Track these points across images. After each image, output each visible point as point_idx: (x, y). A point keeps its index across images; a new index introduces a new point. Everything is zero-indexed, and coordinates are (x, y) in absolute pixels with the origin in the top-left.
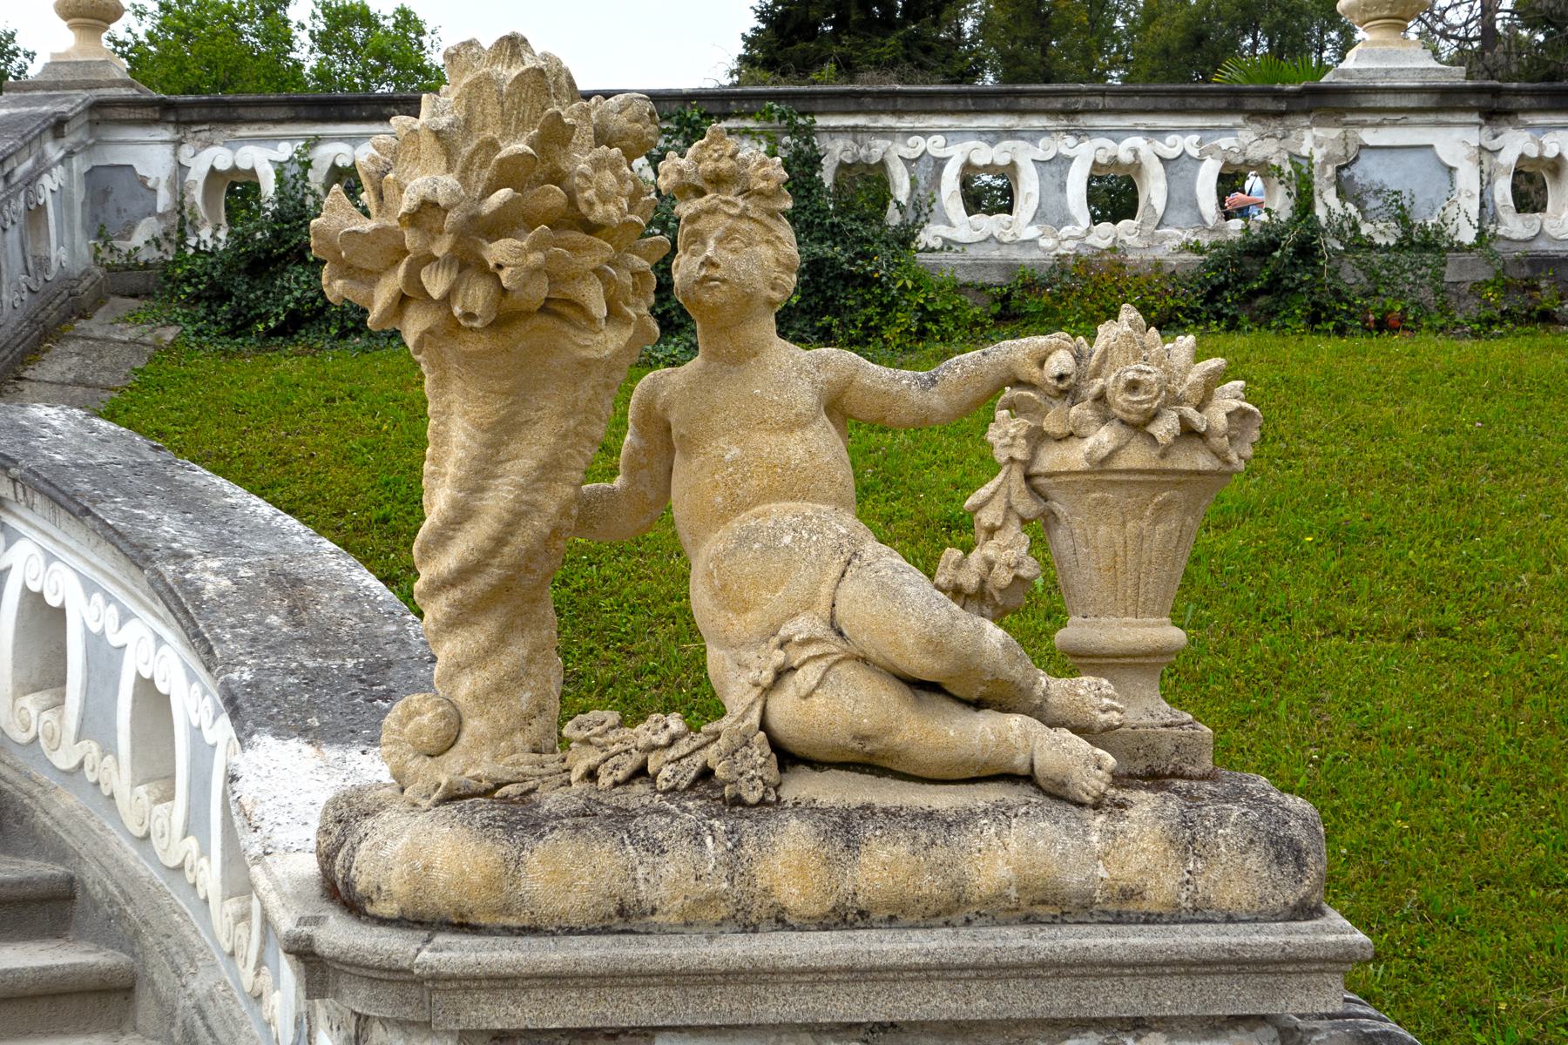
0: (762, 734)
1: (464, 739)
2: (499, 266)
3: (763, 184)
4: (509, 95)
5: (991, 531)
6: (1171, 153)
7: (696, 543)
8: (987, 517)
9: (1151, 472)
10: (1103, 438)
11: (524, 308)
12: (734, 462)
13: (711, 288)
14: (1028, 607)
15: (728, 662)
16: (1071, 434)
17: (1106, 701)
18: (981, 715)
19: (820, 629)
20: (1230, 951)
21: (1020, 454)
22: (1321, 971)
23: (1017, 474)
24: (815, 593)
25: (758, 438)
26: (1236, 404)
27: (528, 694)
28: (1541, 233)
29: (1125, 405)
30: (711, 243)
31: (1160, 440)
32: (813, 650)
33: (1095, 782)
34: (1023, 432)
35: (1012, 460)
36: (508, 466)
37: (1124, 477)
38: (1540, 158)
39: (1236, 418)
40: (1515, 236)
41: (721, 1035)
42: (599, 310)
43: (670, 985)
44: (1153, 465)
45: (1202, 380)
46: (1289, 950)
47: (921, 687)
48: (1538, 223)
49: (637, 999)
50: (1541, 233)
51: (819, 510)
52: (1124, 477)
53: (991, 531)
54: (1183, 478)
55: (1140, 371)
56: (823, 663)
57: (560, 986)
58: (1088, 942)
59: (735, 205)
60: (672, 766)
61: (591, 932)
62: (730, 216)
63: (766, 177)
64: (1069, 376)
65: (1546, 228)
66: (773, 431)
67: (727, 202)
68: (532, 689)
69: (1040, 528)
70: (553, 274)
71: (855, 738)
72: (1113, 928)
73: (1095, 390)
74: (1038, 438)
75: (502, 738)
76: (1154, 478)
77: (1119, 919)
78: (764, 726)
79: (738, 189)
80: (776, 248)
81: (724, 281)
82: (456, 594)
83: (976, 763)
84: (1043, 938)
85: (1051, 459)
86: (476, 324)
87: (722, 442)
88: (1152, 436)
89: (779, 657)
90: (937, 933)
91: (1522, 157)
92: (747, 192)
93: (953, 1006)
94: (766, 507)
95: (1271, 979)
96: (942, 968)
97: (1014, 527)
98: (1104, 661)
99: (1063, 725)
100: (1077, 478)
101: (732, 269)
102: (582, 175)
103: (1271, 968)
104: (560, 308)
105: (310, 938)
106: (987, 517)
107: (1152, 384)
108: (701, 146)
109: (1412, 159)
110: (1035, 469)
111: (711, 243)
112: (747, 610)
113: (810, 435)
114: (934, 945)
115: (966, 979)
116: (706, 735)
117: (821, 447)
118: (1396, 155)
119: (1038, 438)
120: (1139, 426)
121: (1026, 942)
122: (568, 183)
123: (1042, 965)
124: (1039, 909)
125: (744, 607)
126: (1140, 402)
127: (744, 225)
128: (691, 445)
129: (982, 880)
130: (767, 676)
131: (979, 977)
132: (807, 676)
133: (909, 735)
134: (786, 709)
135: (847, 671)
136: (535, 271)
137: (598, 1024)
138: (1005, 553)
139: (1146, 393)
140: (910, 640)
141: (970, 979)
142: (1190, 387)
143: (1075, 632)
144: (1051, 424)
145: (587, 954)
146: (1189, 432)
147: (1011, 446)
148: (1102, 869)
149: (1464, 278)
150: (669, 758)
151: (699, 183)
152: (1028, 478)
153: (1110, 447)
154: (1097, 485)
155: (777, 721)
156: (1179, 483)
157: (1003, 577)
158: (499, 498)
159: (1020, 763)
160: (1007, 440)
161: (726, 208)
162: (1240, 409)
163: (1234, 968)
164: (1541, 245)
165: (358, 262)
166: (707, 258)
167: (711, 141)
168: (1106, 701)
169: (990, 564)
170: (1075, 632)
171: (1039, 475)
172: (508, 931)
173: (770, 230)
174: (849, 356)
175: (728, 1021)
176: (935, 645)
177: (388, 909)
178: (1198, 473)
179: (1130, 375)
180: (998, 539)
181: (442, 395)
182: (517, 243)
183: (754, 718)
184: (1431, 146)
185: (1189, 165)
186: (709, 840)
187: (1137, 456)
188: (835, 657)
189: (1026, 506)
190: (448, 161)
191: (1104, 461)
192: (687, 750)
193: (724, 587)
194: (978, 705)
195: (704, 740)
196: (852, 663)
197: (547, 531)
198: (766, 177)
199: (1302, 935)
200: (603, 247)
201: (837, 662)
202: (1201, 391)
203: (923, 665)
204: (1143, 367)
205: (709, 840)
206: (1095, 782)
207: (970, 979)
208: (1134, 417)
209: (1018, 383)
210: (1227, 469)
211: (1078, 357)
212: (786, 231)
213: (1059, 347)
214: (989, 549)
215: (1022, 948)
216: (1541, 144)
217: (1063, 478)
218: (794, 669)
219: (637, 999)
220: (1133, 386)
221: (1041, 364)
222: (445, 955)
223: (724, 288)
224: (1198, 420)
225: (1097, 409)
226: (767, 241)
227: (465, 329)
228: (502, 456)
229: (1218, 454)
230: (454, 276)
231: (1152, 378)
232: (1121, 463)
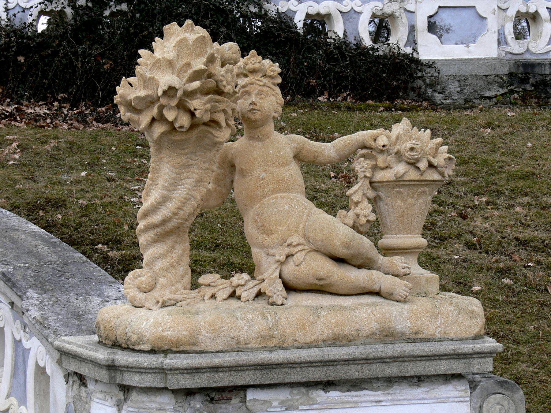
0: (280, 280)
1: (158, 286)
2: (195, 109)
3: (272, 74)
4: (193, 45)
5: (357, 203)
6: (345, 9)
7: (247, 209)
8: (355, 198)
9: (418, 181)
10: (400, 168)
11: (197, 123)
12: (264, 179)
13: (254, 113)
14: (374, 230)
15: (263, 254)
16: (387, 167)
17: (405, 265)
18: (361, 270)
19: (302, 240)
20: (454, 350)
21: (368, 175)
22: (485, 357)
23: (367, 182)
24: (298, 227)
25: (272, 170)
26: (447, 155)
27: (182, 268)
28: (528, 50)
29: (409, 156)
30: (253, 96)
31: (421, 169)
32: (300, 248)
33: (405, 293)
34: (370, 166)
35: (365, 177)
36: (184, 181)
37: (408, 183)
38: (527, 13)
39: (447, 160)
40: (515, 52)
41: (271, 388)
42: (223, 124)
43: (256, 369)
44: (418, 178)
45: (435, 146)
46: (475, 349)
47: (339, 260)
48: (526, 45)
49: (244, 375)
50: (528, 50)
51: (295, 196)
52: (408, 183)
53: (357, 203)
54: (429, 183)
55: (414, 144)
56: (304, 253)
57: (217, 371)
58: (405, 349)
59: (261, 81)
60: (246, 292)
61: (226, 351)
62: (260, 85)
63: (273, 71)
64: (387, 145)
65: (530, 48)
66: (277, 167)
67: (258, 80)
68: (183, 266)
69: (374, 201)
70: (212, 111)
71: (317, 279)
72: (413, 344)
73: (395, 150)
74: (375, 168)
75: (173, 285)
76: (418, 183)
77: (414, 341)
78: (280, 277)
79: (261, 75)
80: (276, 97)
81: (259, 110)
82: (159, 230)
83: (360, 288)
84: (389, 348)
85: (380, 176)
86: (183, 130)
87: (258, 171)
88: (418, 168)
89: (287, 251)
90: (351, 348)
91: (518, 12)
92: (264, 76)
93: (357, 374)
94: (276, 195)
95: (468, 360)
96: (355, 360)
97: (366, 202)
98: (399, 251)
99: (389, 274)
100: (390, 183)
101: (261, 106)
102: (223, 76)
103: (469, 356)
104: (214, 123)
105: (113, 360)
106: (355, 198)
107: (418, 149)
108: (248, 59)
109: (465, 14)
110: (373, 180)
111: (253, 96)
112: (272, 234)
113: (291, 168)
114: (352, 351)
115: (362, 364)
116: (258, 280)
117: (293, 172)
118: (457, 11)
119: (375, 168)
120: (413, 164)
121: (384, 349)
122: (216, 78)
123: (390, 358)
124: (386, 338)
125: (270, 233)
126: (415, 156)
127: (265, 89)
128: (243, 174)
129: (367, 328)
130: (283, 258)
131: (367, 363)
132: (298, 257)
133: (337, 278)
134: (290, 271)
135: (314, 255)
136: (206, 111)
137: (230, 385)
138: (365, 211)
139: (417, 152)
140: (338, 243)
141: (363, 364)
142: (430, 149)
143: (387, 241)
144: (380, 164)
145: (227, 359)
146: (431, 165)
147: (365, 171)
148: (409, 323)
149: (490, 73)
150: (245, 289)
151: (245, 72)
152: (371, 183)
153: (403, 172)
154: (398, 186)
155: (286, 275)
156: (427, 185)
157: (363, 220)
158: (180, 193)
159: (376, 288)
160: (363, 169)
161: (258, 82)
162: (449, 157)
163: (455, 357)
164: (528, 56)
165: (137, 107)
166: (253, 102)
167: (251, 57)
168: (405, 265)
169: (358, 216)
170: (387, 241)
171: (374, 182)
172: (196, 352)
173: (274, 90)
174: (301, 137)
175: (277, 382)
176: (347, 246)
177: (146, 347)
178: (434, 181)
179: (411, 146)
180: (360, 206)
181: (158, 155)
182: (201, 101)
183: (277, 274)
184: (474, 7)
185: (355, 16)
186: (269, 317)
187: (413, 175)
188: (308, 250)
189: (371, 194)
190: (173, 70)
191: (400, 177)
192: (251, 286)
193: (263, 226)
194: (359, 267)
195: (258, 282)
196: (313, 252)
197: (196, 205)
198: (273, 71)
199: (478, 346)
200: (227, 101)
201: (308, 252)
202: (434, 151)
203: (341, 252)
204: (415, 142)
205: (269, 317)
206: (405, 293)
207: (363, 364)
208: (412, 161)
209: (364, 147)
210: (443, 179)
211: (388, 137)
212: (278, 90)
213: (381, 134)
214: (357, 210)
215: (382, 351)
216: (527, 6)
217: (384, 184)
218: (293, 255)
219: (244, 375)
220: (412, 149)
221: (375, 140)
222: (175, 361)
223: (259, 113)
224: (435, 162)
225: (396, 158)
226: (273, 95)
227: (178, 132)
228: (182, 178)
229: (442, 174)
230: (177, 113)
231: (419, 146)
232: (407, 178)
